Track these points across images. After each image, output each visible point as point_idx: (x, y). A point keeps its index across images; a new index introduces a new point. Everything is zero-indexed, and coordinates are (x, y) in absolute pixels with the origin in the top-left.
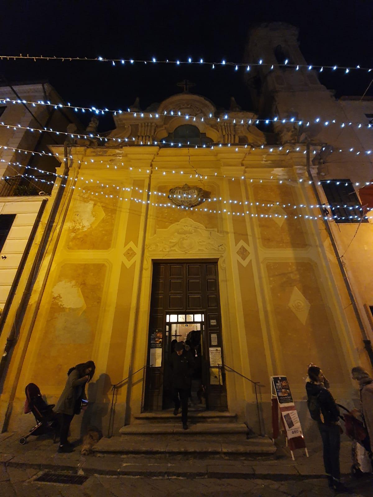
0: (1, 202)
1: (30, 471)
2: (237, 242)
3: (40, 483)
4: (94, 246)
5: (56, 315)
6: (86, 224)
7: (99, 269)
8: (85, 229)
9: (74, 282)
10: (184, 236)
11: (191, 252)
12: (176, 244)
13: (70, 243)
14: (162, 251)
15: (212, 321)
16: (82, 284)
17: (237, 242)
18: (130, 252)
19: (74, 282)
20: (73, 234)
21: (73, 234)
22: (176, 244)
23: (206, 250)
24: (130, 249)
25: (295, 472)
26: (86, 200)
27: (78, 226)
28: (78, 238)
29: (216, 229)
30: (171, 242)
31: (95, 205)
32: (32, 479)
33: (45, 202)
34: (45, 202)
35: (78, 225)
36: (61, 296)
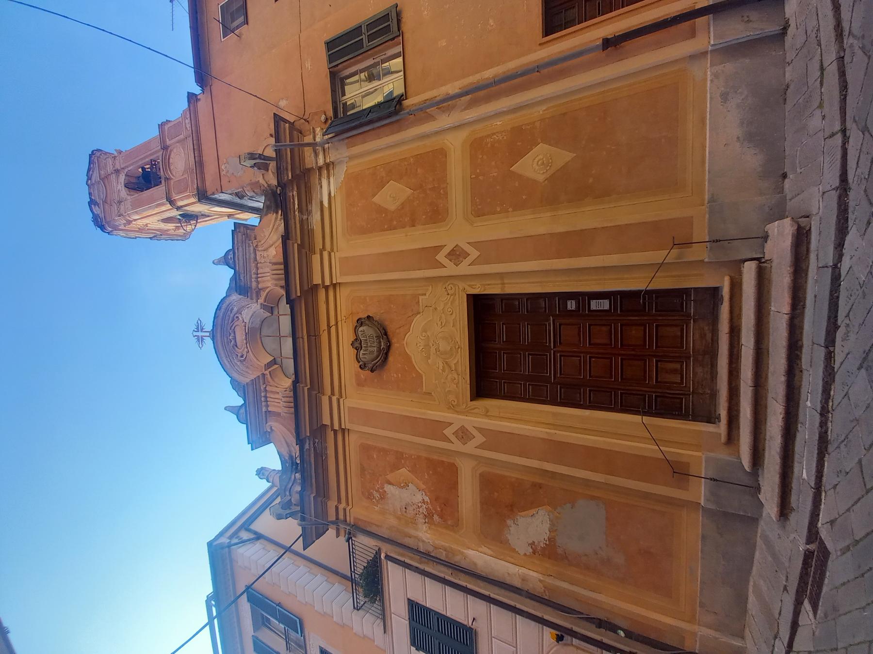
0: (837, 7)
1: (802, 620)
2: (475, 245)
3: (819, 612)
4: (454, 486)
5: (560, 551)
6: (419, 497)
7: (489, 484)
8: (427, 499)
9: (509, 522)
10: (433, 350)
11: (458, 339)
12: (446, 363)
13: (449, 523)
14: (457, 384)
15: (569, 307)
16: (512, 510)
17: (475, 245)
18: (460, 434)
19: (509, 522)
20: (436, 517)
21: (436, 517)
22: (446, 363)
23: (454, 315)
24: (455, 433)
25: (834, 195)
26: (383, 496)
27: (423, 510)
28: (442, 510)
29: (421, 298)
30: (443, 370)
31: (390, 483)
32: (813, 620)
33: (388, 557)
34: (388, 557)
35: (421, 510)
36: (530, 542)
